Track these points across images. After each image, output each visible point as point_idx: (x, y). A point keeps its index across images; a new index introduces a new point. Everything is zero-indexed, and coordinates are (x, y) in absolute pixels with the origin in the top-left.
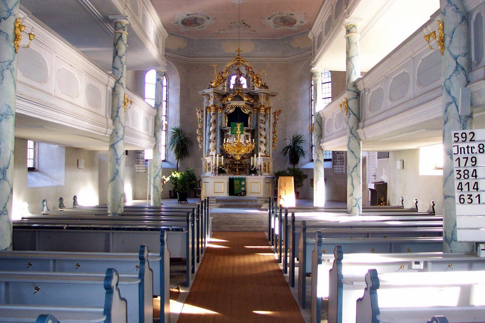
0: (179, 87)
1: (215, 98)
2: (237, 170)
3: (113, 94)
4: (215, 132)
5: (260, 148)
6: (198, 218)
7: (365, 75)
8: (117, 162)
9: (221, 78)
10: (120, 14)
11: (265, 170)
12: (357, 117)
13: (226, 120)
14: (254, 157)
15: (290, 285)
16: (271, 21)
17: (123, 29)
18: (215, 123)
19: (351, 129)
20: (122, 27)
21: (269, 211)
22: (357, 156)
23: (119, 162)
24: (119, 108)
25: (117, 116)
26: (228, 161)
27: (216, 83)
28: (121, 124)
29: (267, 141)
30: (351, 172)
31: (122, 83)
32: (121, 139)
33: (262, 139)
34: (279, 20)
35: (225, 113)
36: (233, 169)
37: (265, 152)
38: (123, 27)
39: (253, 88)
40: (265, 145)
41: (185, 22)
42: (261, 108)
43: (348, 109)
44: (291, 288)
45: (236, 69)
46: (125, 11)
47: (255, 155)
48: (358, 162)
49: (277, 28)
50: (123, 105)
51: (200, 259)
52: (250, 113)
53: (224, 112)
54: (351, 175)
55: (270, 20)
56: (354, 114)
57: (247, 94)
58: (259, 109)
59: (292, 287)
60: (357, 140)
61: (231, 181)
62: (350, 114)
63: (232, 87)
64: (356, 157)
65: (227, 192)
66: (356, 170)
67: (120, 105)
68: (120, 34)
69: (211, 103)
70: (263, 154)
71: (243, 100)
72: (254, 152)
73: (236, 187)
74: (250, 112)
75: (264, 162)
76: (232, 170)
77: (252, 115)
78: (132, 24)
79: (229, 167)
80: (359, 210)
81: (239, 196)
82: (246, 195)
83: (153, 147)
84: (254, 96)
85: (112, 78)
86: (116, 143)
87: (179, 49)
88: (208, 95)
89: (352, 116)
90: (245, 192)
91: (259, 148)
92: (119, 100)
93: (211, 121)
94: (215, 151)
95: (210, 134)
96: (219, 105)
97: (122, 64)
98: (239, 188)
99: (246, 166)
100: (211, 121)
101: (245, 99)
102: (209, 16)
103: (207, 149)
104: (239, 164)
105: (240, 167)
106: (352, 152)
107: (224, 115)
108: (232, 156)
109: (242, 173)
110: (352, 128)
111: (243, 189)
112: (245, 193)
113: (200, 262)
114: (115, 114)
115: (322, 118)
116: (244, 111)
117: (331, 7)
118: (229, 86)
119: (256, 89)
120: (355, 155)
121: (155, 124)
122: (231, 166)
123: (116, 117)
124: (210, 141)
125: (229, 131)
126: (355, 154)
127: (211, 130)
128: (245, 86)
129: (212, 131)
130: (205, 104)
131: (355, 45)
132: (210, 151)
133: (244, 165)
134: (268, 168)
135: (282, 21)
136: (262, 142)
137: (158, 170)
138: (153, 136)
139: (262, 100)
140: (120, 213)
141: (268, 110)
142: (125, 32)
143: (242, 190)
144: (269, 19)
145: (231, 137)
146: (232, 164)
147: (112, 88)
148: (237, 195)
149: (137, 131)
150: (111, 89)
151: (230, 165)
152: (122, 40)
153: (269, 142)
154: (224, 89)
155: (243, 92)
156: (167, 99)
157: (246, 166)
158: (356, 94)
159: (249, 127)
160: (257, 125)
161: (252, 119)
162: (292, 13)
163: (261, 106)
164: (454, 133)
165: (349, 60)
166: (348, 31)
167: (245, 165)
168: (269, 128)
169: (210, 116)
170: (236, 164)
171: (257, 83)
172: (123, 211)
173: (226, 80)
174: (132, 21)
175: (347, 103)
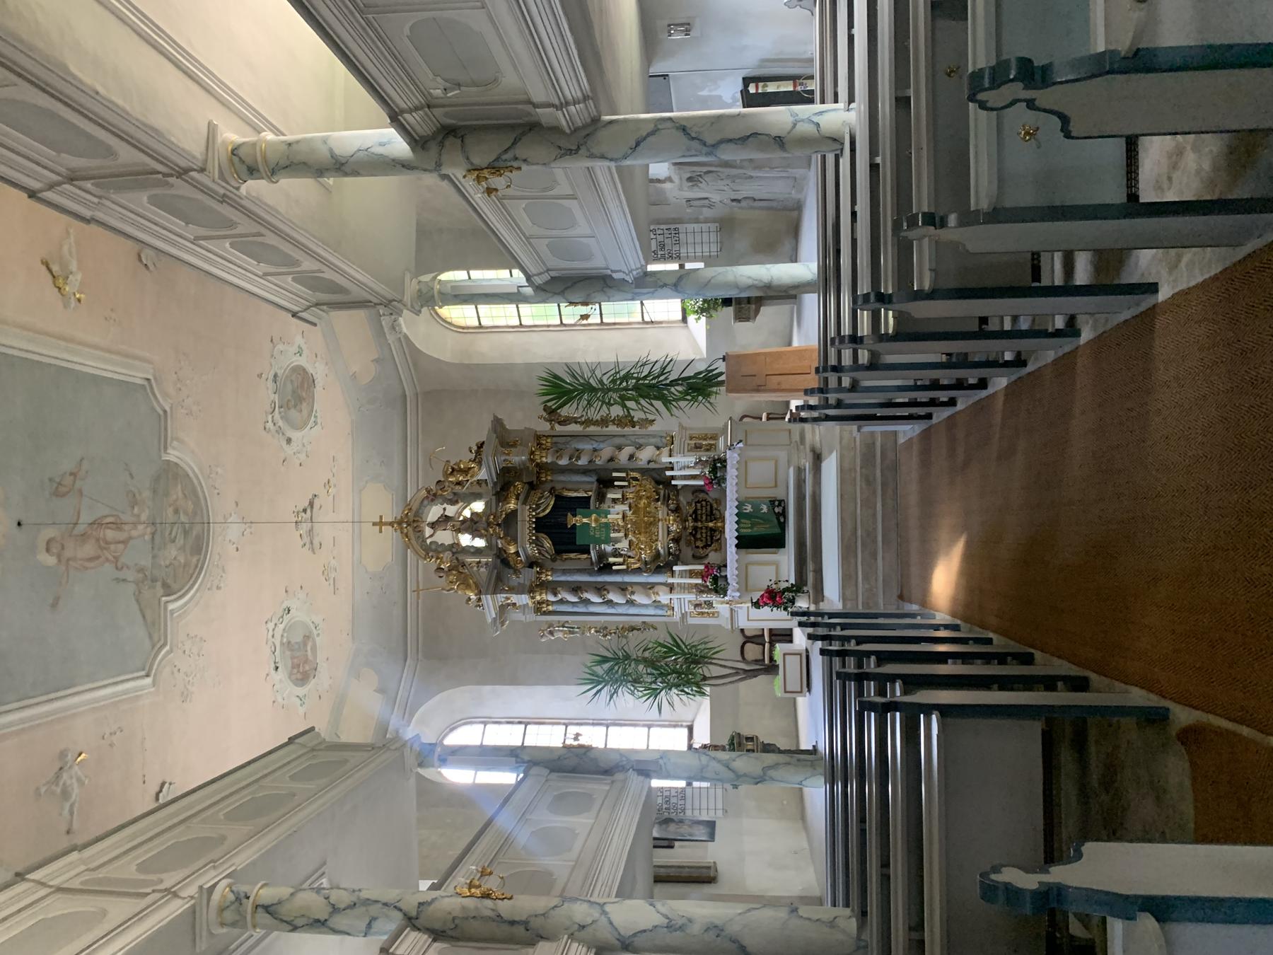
0: (488, 688)
1: (512, 590)
2: (711, 524)
3: (452, 937)
4: (605, 590)
5: (649, 462)
6: (833, 626)
7: (395, 118)
8: (681, 928)
9: (454, 572)
10: (193, 911)
11: (710, 448)
12: (523, 134)
13: (571, 559)
14: (673, 478)
15: (1147, 302)
16: (295, 435)
17: (245, 901)
18: (580, 587)
19: (563, 152)
20: (237, 904)
22: (651, 127)
23: (680, 922)
24: (499, 916)
25: (525, 924)
26: (688, 552)
27: (468, 587)
28: (552, 912)
29: (628, 442)
30: (705, 144)
31: (419, 907)
32: (604, 913)
33: (623, 456)
34: (293, 413)
35: (554, 560)
37: (658, 448)
38: (237, 898)
39: (484, 485)
40: (639, 447)
41: (299, 676)
42: (539, 461)
43: (501, 164)
44: (1164, 294)
46: (184, 894)
47: (668, 473)
48: (672, 124)
49: (319, 422)
50: (488, 903)
51: (1074, 671)
52: (552, 490)
53: (549, 564)
54: (713, 146)
55: (294, 439)
56: (514, 143)
57: (498, 501)
58: (541, 467)
59: (1156, 291)
60: (596, 130)
61: (745, 543)
62: (516, 159)
63: (480, 543)
64: (652, 133)
65: (775, 553)
66: (696, 129)
67: (488, 913)
68: (260, 910)
69: (523, 599)
70: (665, 451)
71: (514, 512)
72: (660, 480)
73: (761, 530)
74: (550, 492)
75: (686, 450)
76: (712, 539)
77: (558, 486)
78: (233, 868)
79: (702, 548)
80: (833, 113)
81: (785, 518)
83: (641, 778)
84: (504, 484)
85: (394, 947)
86: (616, 929)
87: (381, 690)
88: (503, 609)
89: (520, 151)
90: (772, 502)
91: (647, 467)
92: (474, 917)
93: (575, 599)
94: (657, 588)
95: (610, 603)
96: (528, 576)
97: (355, 904)
98: (762, 521)
99: (698, 502)
100: (575, 599)
101: (512, 506)
102: (284, 606)
103: (651, 611)
104: (696, 520)
106: (638, 144)
107: (558, 565)
108: (672, 540)
109: (719, 511)
110: (560, 147)
111: (765, 509)
112: (777, 503)
113: (991, 635)
114: (520, 930)
115: (552, 277)
117: (201, 242)
118: (478, 551)
119: (483, 474)
120: (648, 135)
121: (574, 770)
122: (699, 544)
123: (528, 930)
124: (631, 603)
125: (600, 548)
126: (644, 134)
127: (600, 600)
128: (478, 506)
129: (601, 596)
130: (528, 616)
131: (294, 147)
132: (659, 602)
134: (705, 439)
135: (295, 406)
136: (631, 457)
137: (714, 764)
138: (608, 779)
139: (518, 458)
140: (853, 924)
141: (544, 442)
142: (255, 891)
143: (769, 510)
144: (289, 441)
146: (696, 539)
147: (435, 940)
148: (783, 526)
149: (580, 855)
150: (436, 945)
151: (698, 547)
152: (280, 903)
153: (633, 438)
154: (487, 564)
155: (494, 511)
156: (520, 723)
157: (698, 502)
158: (451, 139)
159: (590, 493)
160: (585, 471)
162: (271, 377)
163: (532, 461)
165: (343, 164)
166: (252, 171)
167: (696, 503)
169: (562, 602)
171: (466, 471)
172: (848, 911)
173: (460, 558)
174: (225, 866)
175: (482, 169)
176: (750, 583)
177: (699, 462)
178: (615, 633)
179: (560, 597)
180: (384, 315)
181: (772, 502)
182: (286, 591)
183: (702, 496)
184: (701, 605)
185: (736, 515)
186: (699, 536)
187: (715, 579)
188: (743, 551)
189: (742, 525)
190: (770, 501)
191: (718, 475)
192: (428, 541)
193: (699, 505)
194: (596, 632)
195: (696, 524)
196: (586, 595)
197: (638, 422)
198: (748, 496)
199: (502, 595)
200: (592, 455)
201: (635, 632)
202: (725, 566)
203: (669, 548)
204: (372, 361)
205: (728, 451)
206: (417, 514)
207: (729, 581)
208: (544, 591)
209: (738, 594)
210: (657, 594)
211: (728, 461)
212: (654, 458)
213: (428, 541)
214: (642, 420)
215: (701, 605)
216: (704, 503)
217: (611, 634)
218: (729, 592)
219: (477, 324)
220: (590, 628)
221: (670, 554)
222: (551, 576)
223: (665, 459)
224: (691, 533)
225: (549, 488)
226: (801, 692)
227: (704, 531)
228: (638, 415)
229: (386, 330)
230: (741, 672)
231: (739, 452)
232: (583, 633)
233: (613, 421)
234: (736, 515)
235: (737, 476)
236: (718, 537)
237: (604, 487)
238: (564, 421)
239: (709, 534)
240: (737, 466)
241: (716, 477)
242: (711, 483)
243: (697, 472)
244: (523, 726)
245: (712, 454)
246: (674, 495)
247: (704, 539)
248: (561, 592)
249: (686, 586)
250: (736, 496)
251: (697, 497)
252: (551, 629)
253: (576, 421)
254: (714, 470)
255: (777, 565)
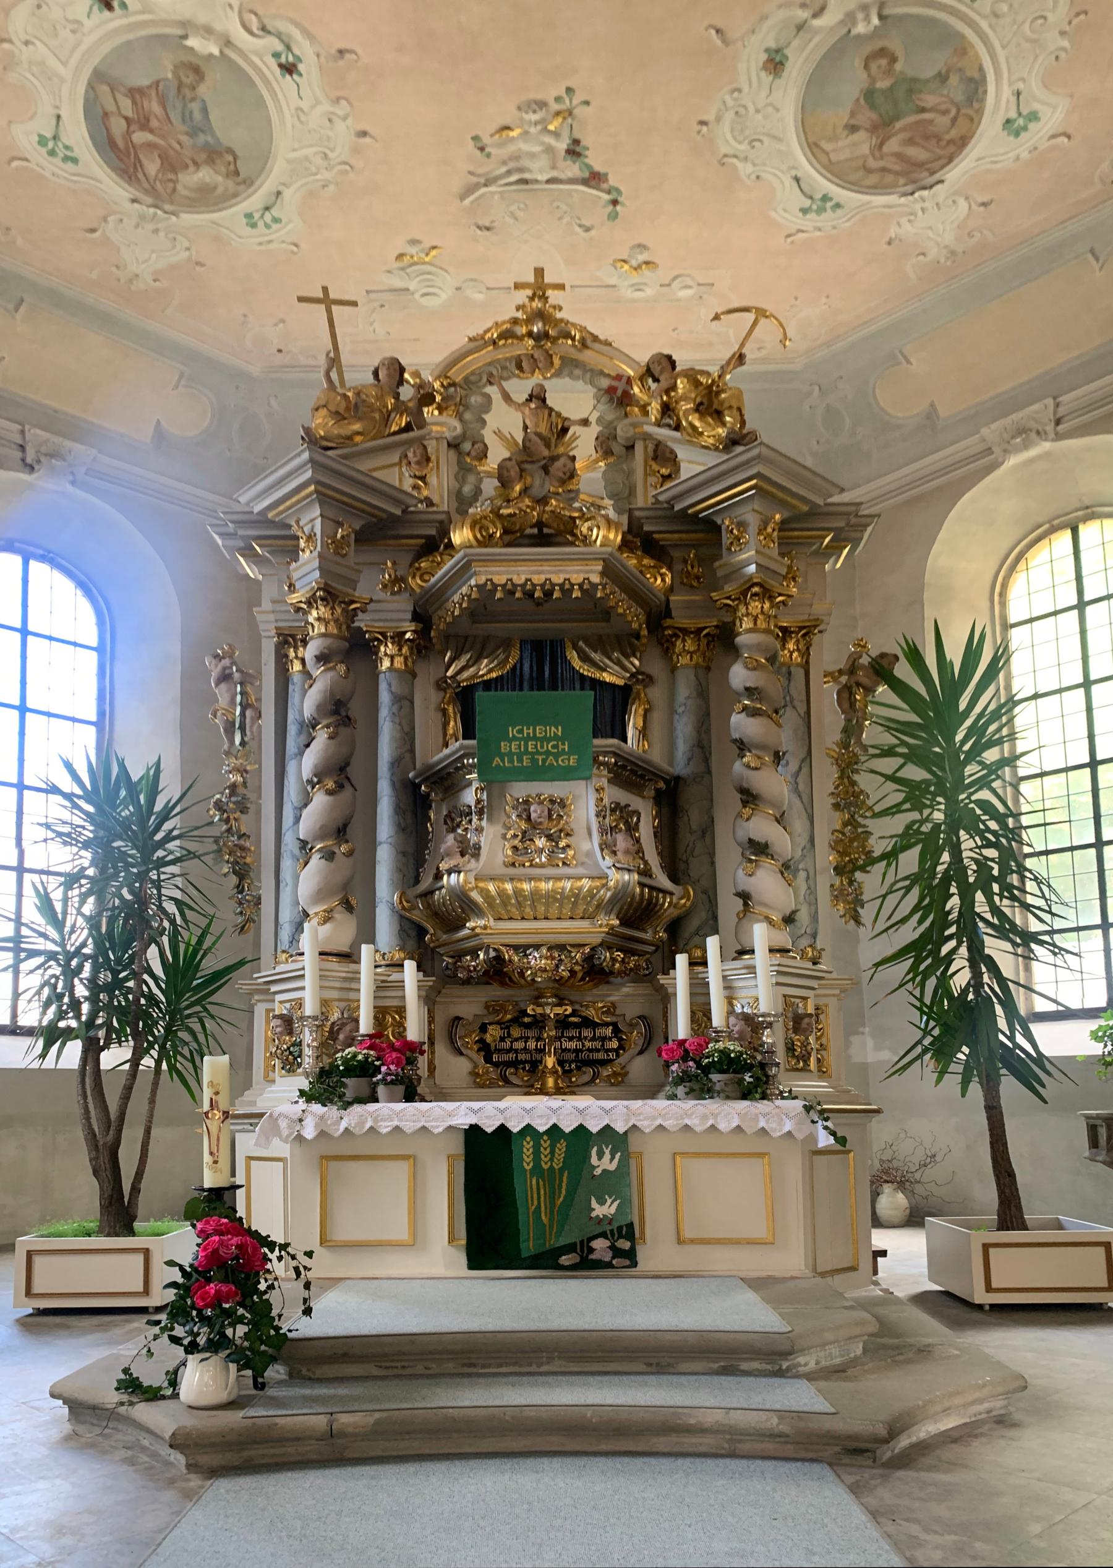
2: (550, 1061)
4: (340, 786)
13: (445, 725)
14: (699, 962)
21: (383, 963)
35: (441, 684)
36: (512, 1056)
45: (521, 397)
65: (451, 1239)
77: (656, 693)
82: (634, 1264)
99: (617, 1031)
104: (562, 1023)
105: (571, 1039)
108: (499, 958)
111: (604, 1209)
112: (624, 1245)
116: (593, 664)
122: (493, 1034)
125: (470, 769)
133: (607, 1024)
143: (599, 1221)
145: (480, 813)
146: (505, 1026)
151: (483, 1028)
157: (617, 1031)
161: (657, 717)
163: (743, 595)
164: (987, 1291)
167: (615, 1025)
168: (805, 770)
170: (539, 1023)
176: (333, 1164)
177: (753, 1024)
178: (229, 830)
179: (317, 672)
180: (1057, 405)
181: (628, 1232)
182: (341, 52)
183: (636, 1037)
184: (290, 1033)
185: (581, 1128)
186: (516, 1032)
187: (365, 1070)
188: (457, 1146)
189: (545, 1143)
190: (630, 1226)
191: (715, 1077)
192: (492, 391)
193: (609, 1031)
194: (233, 787)
195: (551, 1024)
196: (321, 737)
197: (851, 882)
198: (646, 1158)
199: (318, 522)
200: (763, 747)
201: (234, 880)
202: (410, 1096)
203: (474, 953)
204: (932, 405)
205: (798, 1104)
206: (570, 365)
207: (357, 1109)
208: (333, 629)
209: (309, 1133)
210: (326, 920)
211: (763, 1106)
212: (757, 909)
213: (492, 391)
214: (859, 892)
215: (290, 1033)
216: (615, 1044)
217: (227, 821)
218: (316, 1108)
219: (1012, 620)
220: (242, 771)
221: (459, 956)
222: (391, 669)
223: (760, 935)
224: (524, 1013)
225: (648, 671)
226: (29, 1293)
227: (532, 1044)
228: (871, 882)
229: (1015, 417)
230: (110, 1137)
231: (800, 1136)
232: (228, 753)
233: (851, 822)
234: (581, 1128)
235: (713, 1127)
236: (514, 1079)
237: (658, 791)
238: (852, 703)
239: (522, 1057)
240: (750, 1130)
241: (706, 1070)
242: (685, 1057)
243: (718, 1019)
244: (94, 718)
245: (780, 1057)
246: (637, 967)
247: (507, 1044)
248: (330, 675)
249: (352, 995)
250: (646, 1125)
251: (632, 1026)
252: (237, 676)
253: (852, 730)
254: (729, 1064)
255: (414, 1242)
